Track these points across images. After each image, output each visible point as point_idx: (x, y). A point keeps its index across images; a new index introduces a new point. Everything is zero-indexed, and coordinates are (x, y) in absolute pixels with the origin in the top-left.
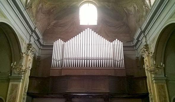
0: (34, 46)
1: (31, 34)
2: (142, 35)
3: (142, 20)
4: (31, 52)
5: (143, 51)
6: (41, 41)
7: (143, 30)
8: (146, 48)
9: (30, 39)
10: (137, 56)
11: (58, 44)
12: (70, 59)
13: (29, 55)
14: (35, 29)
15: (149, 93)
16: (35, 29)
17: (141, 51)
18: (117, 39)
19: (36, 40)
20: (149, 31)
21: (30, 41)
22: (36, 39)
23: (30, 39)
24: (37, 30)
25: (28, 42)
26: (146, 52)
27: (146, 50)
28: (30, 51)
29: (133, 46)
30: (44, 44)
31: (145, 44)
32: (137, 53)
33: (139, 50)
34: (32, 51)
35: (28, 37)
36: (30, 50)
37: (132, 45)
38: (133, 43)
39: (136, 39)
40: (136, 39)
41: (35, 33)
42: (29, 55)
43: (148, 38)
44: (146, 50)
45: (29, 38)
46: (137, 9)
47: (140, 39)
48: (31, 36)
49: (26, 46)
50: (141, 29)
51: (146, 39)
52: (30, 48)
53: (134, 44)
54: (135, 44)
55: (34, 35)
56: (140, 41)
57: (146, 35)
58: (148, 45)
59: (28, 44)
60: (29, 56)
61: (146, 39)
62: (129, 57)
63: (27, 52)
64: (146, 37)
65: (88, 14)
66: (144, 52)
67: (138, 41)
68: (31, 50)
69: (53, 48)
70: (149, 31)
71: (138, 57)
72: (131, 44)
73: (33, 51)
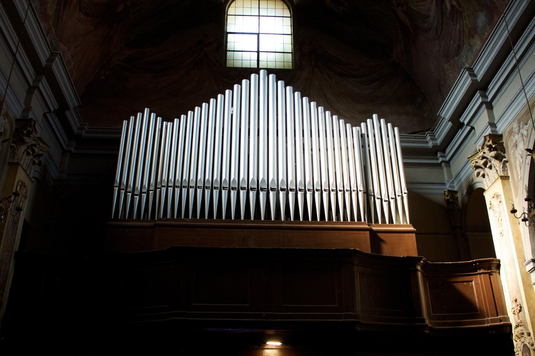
0: (41, 130)
1: (34, 81)
2: (477, 100)
3: (471, 46)
4: (28, 154)
5: (481, 162)
6: (72, 117)
7: (479, 78)
8: (495, 149)
9: (28, 102)
10: (448, 187)
11: (142, 128)
12: (189, 187)
13: (18, 164)
14: (50, 60)
15: (510, 326)
16: (50, 60)
17: (473, 164)
18: (375, 116)
19: (52, 109)
20: (519, 61)
21: (28, 109)
22: (53, 105)
23: (28, 102)
24: (58, 68)
25: (16, 112)
26: (495, 162)
27: (497, 157)
28: (23, 148)
29: (433, 152)
30: (84, 134)
31: (489, 131)
32: (450, 176)
33: (456, 165)
34: (33, 151)
35: (22, 91)
36: (24, 142)
37: (430, 144)
38: (433, 139)
39: (449, 121)
40: (448, 117)
41: (47, 80)
42: (18, 164)
43: (497, 111)
44: (493, 153)
45: (22, 101)
46: (452, 6)
47: (465, 118)
48: (31, 89)
49: (8, 127)
50: (473, 75)
51: (491, 116)
52: (26, 139)
53: (439, 142)
54: (442, 143)
55: (44, 85)
56: (463, 123)
57: (490, 97)
58: (501, 136)
59: (17, 120)
60: (20, 169)
61: (491, 116)
62: (419, 191)
63: (14, 154)
64: (490, 106)
65: (259, 32)
66: (485, 164)
67: (457, 125)
68: (32, 147)
69: (118, 150)
70: (519, 61)
71: (456, 192)
72: (427, 142)
73: (36, 150)
